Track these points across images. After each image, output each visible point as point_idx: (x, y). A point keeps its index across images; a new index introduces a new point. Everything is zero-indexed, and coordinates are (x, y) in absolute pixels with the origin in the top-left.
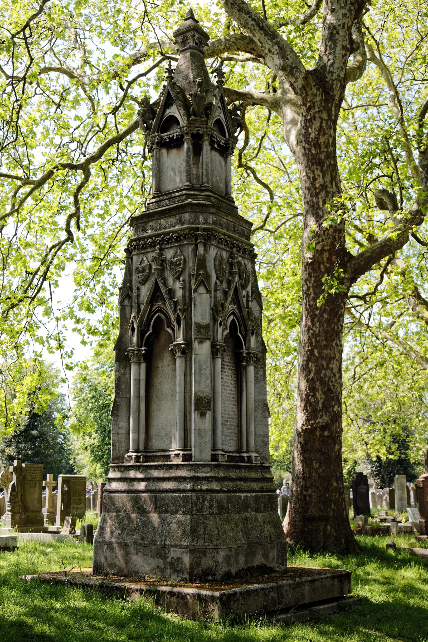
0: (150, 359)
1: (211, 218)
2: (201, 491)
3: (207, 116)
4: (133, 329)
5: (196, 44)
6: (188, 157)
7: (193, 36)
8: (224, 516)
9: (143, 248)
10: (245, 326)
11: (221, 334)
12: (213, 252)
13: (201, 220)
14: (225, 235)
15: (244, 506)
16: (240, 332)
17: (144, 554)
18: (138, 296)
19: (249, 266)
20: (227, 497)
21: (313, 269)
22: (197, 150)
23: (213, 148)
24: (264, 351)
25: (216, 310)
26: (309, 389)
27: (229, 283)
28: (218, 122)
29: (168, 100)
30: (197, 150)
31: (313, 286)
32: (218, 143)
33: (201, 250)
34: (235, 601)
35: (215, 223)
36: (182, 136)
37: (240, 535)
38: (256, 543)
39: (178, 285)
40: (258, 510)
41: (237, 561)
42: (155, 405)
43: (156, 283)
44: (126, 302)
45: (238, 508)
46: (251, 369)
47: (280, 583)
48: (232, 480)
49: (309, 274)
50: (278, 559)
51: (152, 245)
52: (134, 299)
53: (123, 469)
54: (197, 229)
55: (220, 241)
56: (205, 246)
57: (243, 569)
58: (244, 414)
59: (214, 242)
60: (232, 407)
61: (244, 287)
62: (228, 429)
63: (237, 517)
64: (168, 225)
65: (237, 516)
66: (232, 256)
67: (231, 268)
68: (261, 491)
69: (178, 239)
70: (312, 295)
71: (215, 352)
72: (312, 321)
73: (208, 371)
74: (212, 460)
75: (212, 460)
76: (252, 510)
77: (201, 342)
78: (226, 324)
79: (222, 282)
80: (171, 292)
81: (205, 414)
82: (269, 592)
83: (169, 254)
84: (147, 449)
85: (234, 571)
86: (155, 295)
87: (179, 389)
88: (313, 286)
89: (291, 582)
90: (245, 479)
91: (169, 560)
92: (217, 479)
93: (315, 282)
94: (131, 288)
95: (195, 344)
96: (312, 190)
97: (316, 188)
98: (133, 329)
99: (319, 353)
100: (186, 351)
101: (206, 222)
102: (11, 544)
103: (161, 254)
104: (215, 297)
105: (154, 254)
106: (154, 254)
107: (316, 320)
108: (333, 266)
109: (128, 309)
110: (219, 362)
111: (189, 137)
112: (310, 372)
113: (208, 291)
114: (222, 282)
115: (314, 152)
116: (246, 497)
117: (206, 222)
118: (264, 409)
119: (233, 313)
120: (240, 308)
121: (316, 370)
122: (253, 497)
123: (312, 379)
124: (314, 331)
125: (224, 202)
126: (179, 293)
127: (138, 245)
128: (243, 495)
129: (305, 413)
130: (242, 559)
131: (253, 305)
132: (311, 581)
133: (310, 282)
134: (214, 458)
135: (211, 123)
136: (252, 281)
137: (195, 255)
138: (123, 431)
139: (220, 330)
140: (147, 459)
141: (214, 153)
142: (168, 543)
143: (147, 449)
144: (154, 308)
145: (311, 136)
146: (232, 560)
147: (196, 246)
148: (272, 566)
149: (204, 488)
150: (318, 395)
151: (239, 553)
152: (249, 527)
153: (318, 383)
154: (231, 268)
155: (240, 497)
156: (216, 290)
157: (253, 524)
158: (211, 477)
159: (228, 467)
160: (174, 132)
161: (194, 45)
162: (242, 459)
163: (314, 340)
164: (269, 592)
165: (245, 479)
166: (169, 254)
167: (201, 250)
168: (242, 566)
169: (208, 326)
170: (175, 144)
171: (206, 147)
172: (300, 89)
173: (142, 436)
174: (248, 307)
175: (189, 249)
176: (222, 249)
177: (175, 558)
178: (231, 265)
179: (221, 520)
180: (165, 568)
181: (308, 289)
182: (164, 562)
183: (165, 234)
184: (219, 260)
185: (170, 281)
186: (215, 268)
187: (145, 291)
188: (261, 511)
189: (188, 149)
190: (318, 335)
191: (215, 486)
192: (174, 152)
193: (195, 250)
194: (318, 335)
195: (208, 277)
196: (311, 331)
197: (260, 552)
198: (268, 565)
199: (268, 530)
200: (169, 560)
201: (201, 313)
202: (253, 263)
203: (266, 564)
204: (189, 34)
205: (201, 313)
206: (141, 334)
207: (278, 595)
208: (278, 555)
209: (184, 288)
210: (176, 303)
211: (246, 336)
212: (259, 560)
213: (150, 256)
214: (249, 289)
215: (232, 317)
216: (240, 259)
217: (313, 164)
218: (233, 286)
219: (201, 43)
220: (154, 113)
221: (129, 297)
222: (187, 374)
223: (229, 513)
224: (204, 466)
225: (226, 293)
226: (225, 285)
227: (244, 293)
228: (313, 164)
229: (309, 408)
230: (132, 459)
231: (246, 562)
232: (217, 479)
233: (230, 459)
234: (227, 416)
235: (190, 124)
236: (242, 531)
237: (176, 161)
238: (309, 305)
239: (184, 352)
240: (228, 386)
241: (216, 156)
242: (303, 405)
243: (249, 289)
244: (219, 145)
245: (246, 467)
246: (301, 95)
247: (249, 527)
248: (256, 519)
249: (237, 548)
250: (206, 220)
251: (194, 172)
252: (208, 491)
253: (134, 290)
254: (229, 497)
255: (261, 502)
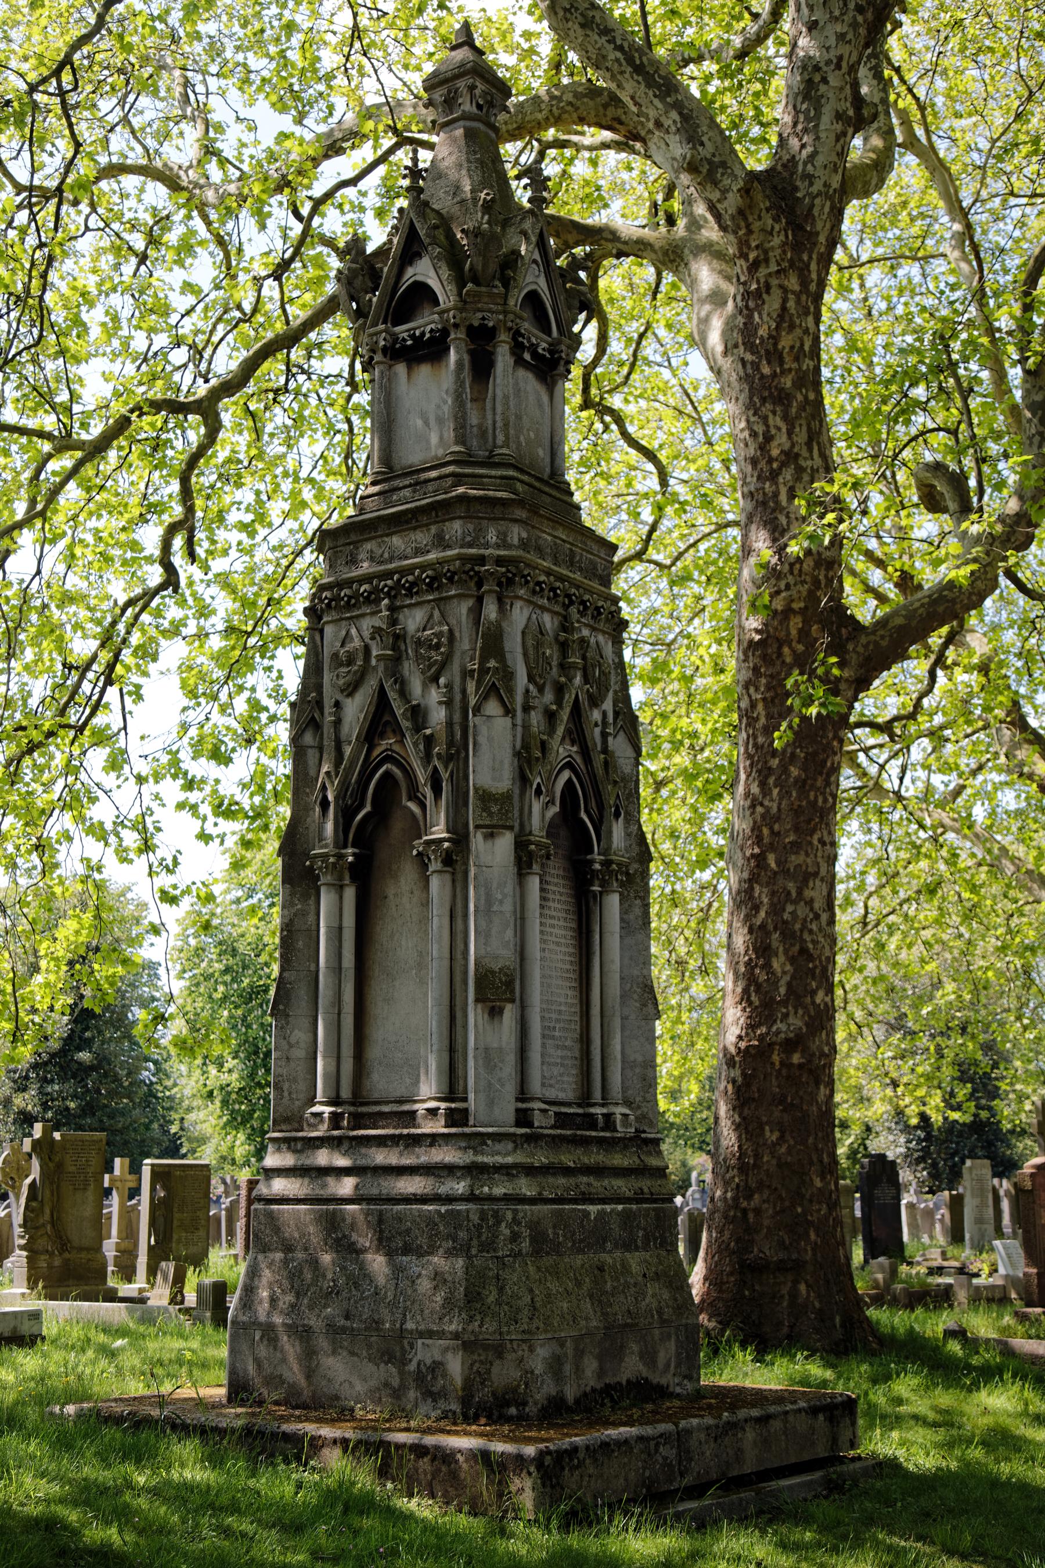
0: (365, 877)
1: (516, 533)
2: (491, 1199)
3: (506, 283)
4: (325, 804)
5: (479, 107)
6: (459, 382)
7: (472, 88)
8: (548, 1261)
9: (349, 606)
10: (598, 795)
11: (540, 815)
12: (519, 615)
13: (492, 536)
14: (548, 573)
15: (596, 1236)
16: (587, 811)
17: (352, 1354)
18: (338, 723)
19: (608, 650)
20: (553, 1212)
21: (764, 657)
22: (481, 367)
23: (519, 362)
24: (645, 857)
25: (528, 757)
26: (755, 949)
27: (560, 690)
28: (533, 298)
29: (410, 244)
30: (481, 367)
31: (764, 699)
32: (533, 349)
33: (491, 610)
34: (573, 1468)
35: (524, 545)
36: (445, 332)
37: (587, 1306)
38: (626, 1325)
39: (435, 696)
40: (629, 1246)
41: (578, 1370)
42: (377, 990)
43: (382, 692)
44: (308, 738)
45: (581, 1241)
46: (613, 902)
47: (683, 1424)
48: (567, 1171)
49: (756, 670)
50: (678, 1365)
51: (372, 599)
52: (328, 730)
53: (299, 1146)
54: (482, 560)
55: (538, 588)
56: (500, 601)
57: (593, 1390)
58: (595, 1011)
59: (522, 592)
60: (566, 995)
61: (595, 701)
62: (558, 1047)
63: (579, 1262)
64: (411, 550)
65: (579, 1260)
66: (566, 626)
67: (564, 655)
68: (639, 1198)
69: (434, 584)
70: (763, 720)
71: (524, 858)
72: (763, 784)
73: (508, 907)
74: (518, 1124)
75: (518, 1124)
76: (616, 1246)
77: (490, 836)
78: (551, 792)
79: (541, 689)
80: (418, 714)
81: (501, 1011)
82: (657, 1445)
83: (413, 620)
84: (358, 1098)
85: (570, 1394)
86: (380, 721)
87: (438, 950)
88: (764, 699)
89: (709, 1421)
90: (598, 1171)
91: (412, 1367)
92: (530, 1171)
93: (768, 688)
94: (319, 704)
95: (477, 841)
96: (763, 464)
97: (771, 460)
98: (325, 804)
99: (778, 863)
100: (455, 857)
101: (503, 543)
102: (26, 1328)
103: (393, 622)
104: (526, 727)
105: (376, 622)
106: (376, 622)
107: (771, 781)
108: (813, 650)
109: (312, 756)
110: (534, 883)
111: (461, 334)
112: (756, 908)
113: (508, 711)
114: (541, 689)
115: (766, 370)
116: (601, 1214)
117: (503, 543)
118: (646, 1000)
119: (569, 765)
120: (585, 752)
121: (772, 904)
122: (619, 1214)
123: (763, 927)
124: (768, 810)
125: (547, 494)
126: (438, 716)
127: (337, 598)
128: (594, 1209)
129: (744, 1010)
130: (591, 1366)
131: (619, 744)
132: (758, 1420)
133: (757, 690)
134: (523, 1118)
135: (515, 300)
136: (614, 686)
137: (477, 622)
138: (299, 1053)
139: (536, 807)
140: (358, 1120)
141: (522, 373)
142: (410, 1325)
143: (358, 1098)
144: (376, 753)
145: (760, 332)
146: (568, 1368)
147: (480, 600)
148: (663, 1381)
149: (499, 1191)
150: (776, 965)
151: (583, 1352)
152: (608, 1287)
153: (776, 936)
154: (564, 655)
155: (586, 1214)
156: (527, 709)
157: (617, 1279)
158: (515, 1166)
159: (556, 1142)
160: (425, 323)
161: (474, 110)
162: (590, 1121)
163: (766, 831)
164: (657, 1445)
165: (598, 1171)
166: (413, 620)
167: (491, 610)
168: (592, 1383)
169: (507, 797)
170: (428, 351)
171: (503, 358)
172: (733, 217)
173: (348, 1066)
174: (605, 750)
175: (462, 609)
176: (543, 608)
177: (428, 1362)
178: (564, 647)
179: (539, 1269)
180: (403, 1388)
181: (753, 705)
182: (402, 1373)
183: (403, 572)
184: (534, 635)
185: (416, 686)
186: (525, 654)
187: (355, 711)
188: (637, 1249)
189: (460, 364)
190: (777, 819)
191: (526, 1187)
192: (424, 370)
193: (477, 611)
194: (777, 819)
195: (508, 676)
196: (759, 809)
197: (635, 1348)
198: (655, 1379)
199: (654, 1296)
200: (412, 1367)
201: (491, 765)
202: (618, 643)
203: (651, 1377)
204: (462, 84)
205: (491, 765)
206: (346, 815)
207: (679, 1454)
208: (678, 1355)
209: (448, 704)
210: (429, 741)
211: (601, 821)
212: (631, 1367)
213: (367, 624)
214: (608, 705)
215: (566, 774)
216: (586, 632)
217: (764, 400)
218: (569, 698)
219: (491, 104)
220: (375, 275)
221: (315, 725)
222: (456, 914)
223: (559, 1254)
224: (497, 1137)
225: (551, 717)
226: (549, 697)
227: (596, 715)
228: (764, 400)
229: (754, 998)
230: (322, 1121)
231: (601, 1373)
232: (530, 1171)
233: (562, 1120)
234: (554, 1016)
235: (464, 303)
236: (591, 1296)
237: (430, 393)
238: (755, 745)
239: (448, 860)
240: (558, 944)
241: (528, 380)
242: (739, 990)
243: (608, 705)
244: (535, 354)
245: (600, 1141)
246: (735, 233)
247: (608, 1287)
248: (625, 1267)
249: (578, 1340)
250: (503, 536)
251: (474, 419)
252: (507, 1199)
253: (328, 708)
254: (559, 1213)
255: (638, 1227)
